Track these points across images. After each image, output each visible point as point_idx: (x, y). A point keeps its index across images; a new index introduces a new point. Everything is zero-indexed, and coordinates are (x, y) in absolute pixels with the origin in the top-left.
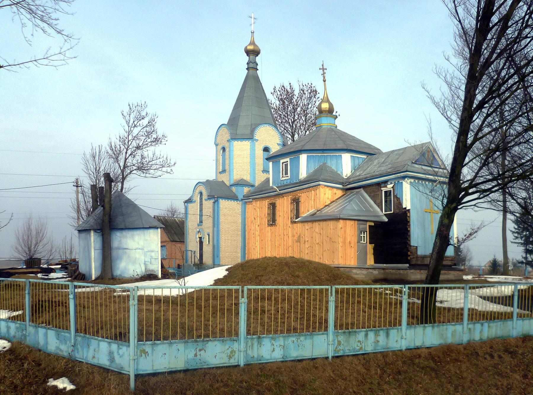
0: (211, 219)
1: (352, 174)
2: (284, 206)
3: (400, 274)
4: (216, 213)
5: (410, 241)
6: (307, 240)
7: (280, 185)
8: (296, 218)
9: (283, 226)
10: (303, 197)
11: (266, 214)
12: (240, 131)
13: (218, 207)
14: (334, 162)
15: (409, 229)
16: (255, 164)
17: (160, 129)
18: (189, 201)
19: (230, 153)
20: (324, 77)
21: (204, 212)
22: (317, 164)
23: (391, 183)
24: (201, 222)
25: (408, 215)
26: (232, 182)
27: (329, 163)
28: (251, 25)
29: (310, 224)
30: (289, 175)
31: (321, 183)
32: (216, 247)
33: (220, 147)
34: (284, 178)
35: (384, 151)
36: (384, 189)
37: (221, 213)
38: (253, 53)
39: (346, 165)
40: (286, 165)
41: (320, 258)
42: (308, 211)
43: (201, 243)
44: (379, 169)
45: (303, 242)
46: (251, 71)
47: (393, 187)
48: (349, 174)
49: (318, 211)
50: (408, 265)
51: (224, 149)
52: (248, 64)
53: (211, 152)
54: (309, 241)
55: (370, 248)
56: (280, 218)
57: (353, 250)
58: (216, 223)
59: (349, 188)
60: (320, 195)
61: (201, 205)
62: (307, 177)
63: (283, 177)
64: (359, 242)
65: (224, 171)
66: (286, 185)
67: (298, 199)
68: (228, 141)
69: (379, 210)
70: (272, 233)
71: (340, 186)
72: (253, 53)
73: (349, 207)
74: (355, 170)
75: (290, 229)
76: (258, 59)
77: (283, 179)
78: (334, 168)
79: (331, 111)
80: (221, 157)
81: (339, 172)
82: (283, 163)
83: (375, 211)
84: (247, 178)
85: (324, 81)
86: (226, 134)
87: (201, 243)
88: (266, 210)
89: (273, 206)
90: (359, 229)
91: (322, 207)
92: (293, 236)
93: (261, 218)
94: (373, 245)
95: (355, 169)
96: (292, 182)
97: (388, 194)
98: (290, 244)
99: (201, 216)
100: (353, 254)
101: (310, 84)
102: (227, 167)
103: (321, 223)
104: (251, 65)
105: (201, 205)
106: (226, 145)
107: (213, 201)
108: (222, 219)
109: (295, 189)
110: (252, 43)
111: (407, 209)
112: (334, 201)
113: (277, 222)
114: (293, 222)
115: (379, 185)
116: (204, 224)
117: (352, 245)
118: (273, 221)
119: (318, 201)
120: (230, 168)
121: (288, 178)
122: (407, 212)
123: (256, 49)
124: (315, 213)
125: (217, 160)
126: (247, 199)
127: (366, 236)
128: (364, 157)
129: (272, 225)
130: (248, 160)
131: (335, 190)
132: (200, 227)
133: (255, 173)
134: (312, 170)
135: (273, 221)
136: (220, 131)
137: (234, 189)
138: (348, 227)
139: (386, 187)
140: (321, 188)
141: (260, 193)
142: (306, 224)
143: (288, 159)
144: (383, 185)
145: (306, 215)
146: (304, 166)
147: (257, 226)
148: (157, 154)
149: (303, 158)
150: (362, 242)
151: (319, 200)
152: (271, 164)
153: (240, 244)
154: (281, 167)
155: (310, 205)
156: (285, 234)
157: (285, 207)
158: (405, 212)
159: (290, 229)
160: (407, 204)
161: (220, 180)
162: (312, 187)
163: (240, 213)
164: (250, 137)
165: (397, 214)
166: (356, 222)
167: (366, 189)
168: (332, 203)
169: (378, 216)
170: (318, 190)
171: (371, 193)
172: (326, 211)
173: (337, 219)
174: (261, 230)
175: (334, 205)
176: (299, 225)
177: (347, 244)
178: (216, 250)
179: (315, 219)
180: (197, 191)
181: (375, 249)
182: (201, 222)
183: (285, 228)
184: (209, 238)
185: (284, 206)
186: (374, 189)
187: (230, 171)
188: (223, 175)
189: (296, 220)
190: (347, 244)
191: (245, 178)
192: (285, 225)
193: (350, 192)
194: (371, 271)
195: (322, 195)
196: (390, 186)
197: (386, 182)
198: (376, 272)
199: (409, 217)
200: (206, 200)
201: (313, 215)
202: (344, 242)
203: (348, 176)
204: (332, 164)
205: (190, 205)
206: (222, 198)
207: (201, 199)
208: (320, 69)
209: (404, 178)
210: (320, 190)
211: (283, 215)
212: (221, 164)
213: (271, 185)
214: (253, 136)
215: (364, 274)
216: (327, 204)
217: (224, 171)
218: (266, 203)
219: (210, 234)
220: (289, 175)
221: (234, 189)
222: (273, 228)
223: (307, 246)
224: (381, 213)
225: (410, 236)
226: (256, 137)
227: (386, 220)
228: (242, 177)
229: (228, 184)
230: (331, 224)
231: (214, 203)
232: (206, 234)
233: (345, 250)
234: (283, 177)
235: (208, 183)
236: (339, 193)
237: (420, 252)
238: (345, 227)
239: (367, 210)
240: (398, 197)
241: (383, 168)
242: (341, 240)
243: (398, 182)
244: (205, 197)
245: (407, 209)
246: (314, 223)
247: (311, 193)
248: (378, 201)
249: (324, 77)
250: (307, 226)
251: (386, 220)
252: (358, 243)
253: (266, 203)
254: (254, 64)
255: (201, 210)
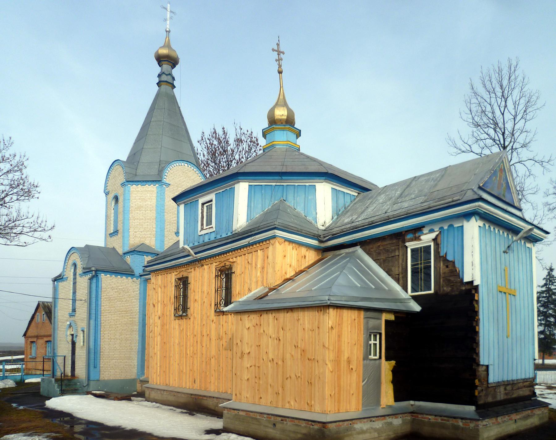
0: (86, 305)
1: (335, 222)
2: (204, 281)
3: (456, 428)
4: (94, 295)
5: (478, 354)
6: (247, 351)
7: (196, 244)
8: (226, 305)
9: (202, 320)
10: (240, 264)
11: (173, 297)
12: (142, 170)
13: (97, 286)
14: (300, 198)
15: (477, 329)
16: (165, 221)
17: (32, 174)
18: (58, 279)
19: (124, 204)
20: (280, 66)
21: (79, 296)
22: (267, 202)
23: (432, 231)
24: (74, 310)
25: (476, 298)
26: (127, 249)
27: (290, 202)
28: (165, 20)
29: (254, 318)
30: (214, 224)
31: (278, 233)
32: (92, 351)
33: (111, 196)
34: (206, 232)
35: (380, 187)
36: (411, 245)
37: (104, 296)
38: (167, 60)
39: (323, 206)
40: (210, 208)
41: (277, 394)
42: (250, 290)
43: (73, 344)
44: (396, 207)
45: (239, 355)
46: (163, 87)
47: (435, 240)
48: (329, 222)
49: (271, 290)
50: (473, 408)
51: (116, 198)
52: (159, 76)
53: (98, 205)
54: (252, 354)
55: (387, 368)
56: (196, 304)
57: (354, 376)
58: (94, 313)
59: (329, 247)
60: (274, 258)
61: (75, 283)
62: (247, 226)
63: (202, 229)
64: (366, 358)
65: (116, 232)
66: (208, 244)
67: (231, 268)
68: (123, 185)
69: (397, 288)
70: (181, 331)
71: (314, 242)
72: (167, 60)
73: (341, 281)
74: (338, 215)
75: (213, 326)
76: (175, 72)
77: (204, 232)
78: (300, 209)
79: (289, 122)
80: (113, 211)
81: (310, 218)
82: (203, 204)
83: (391, 290)
84: (151, 242)
85: (280, 72)
86: (120, 176)
87: (73, 344)
88: (171, 291)
89: (184, 283)
90: (367, 328)
91: (278, 283)
92: (220, 338)
93: (165, 305)
94: (393, 363)
95: (338, 214)
96: (219, 237)
97: (421, 254)
98: (213, 353)
99: (74, 301)
100: (354, 385)
101: (250, 132)
102: (120, 227)
103: (281, 316)
104: (164, 78)
105: (75, 283)
106: (120, 192)
107: (89, 276)
108: (105, 305)
109: (223, 251)
110: (167, 45)
111: (475, 284)
112: (301, 272)
113: (190, 312)
114: (219, 313)
115: (399, 237)
116: (77, 313)
117: (353, 366)
118: (182, 309)
119: (270, 271)
120: (123, 226)
121: (211, 230)
122: (473, 292)
123: (172, 54)
124: (266, 295)
125: (107, 217)
126: (148, 272)
127: (379, 344)
128: (353, 193)
129: (181, 317)
130: (153, 214)
131: (303, 250)
132: (72, 318)
133: (163, 236)
134: (257, 214)
135: (182, 309)
136: (113, 173)
137: (129, 259)
138: (345, 325)
139: (418, 239)
140: (277, 244)
141: (163, 262)
142: (245, 317)
143: (212, 196)
144: (409, 236)
145: (244, 298)
146: (243, 205)
147: (157, 318)
148: (23, 212)
149: (242, 189)
150: (372, 357)
151: (274, 268)
152: (182, 207)
153: (136, 346)
154: (200, 211)
155: (254, 280)
156: (205, 334)
157: (206, 284)
158: (470, 290)
159: (213, 326)
160: (472, 271)
161: (110, 246)
162: (259, 242)
163: (138, 297)
164: (158, 180)
165: (446, 295)
166: (362, 313)
167: (368, 247)
168: (298, 274)
169: (401, 301)
170: (271, 248)
171: (379, 254)
172: (287, 290)
173: (323, 307)
174: (163, 325)
175: (303, 278)
176: (231, 318)
177: (344, 364)
178: (92, 356)
179: (264, 306)
180: (71, 262)
181: (394, 371)
182: (74, 310)
183: (204, 323)
184: (84, 336)
185: (204, 281)
186: (386, 246)
187: (123, 232)
188: (115, 238)
189: (225, 309)
190: (344, 364)
191: (147, 242)
192: (205, 318)
193: (330, 254)
194: (389, 420)
195: (279, 259)
196: (427, 238)
197: (417, 230)
198: (397, 422)
199: (477, 302)
200: (81, 276)
201: (261, 298)
202: (337, 361)
203: (327, 225)
204: (296, 202)
205: (61, 285)
206: (106, 272)
207: (75, 274)
208: (273, 50)
209: (467, 216)
210: (274, 249)
211: (202, 299)
212: (112, 223)
213: (181, 245)
214: (161, 177)
215: (376, 430)
216: (288, 276)
217: (116, 232)
218: (172, 277)
219: (85, 331)
220: (214, 224)
221: (129, 259)
222: (183, 322)
223: (247, 363)
224: (403, 295)
225: (478, 344)
226: (166, 180)
227: (416, 308)
228: (142, 241)
229: (120, 252)
230: (307, 318)
231: (91, 279)
232: (80, 330)
233: (339, 378)
234: (202, 229)
235: (88, 251)
236: (311, 256)
237: (492, 379)
238: (340, 325)
239: (378, 288)
240: (450, 258)
241: (406, 205)
242: (330, 356)
243: (451, 226)
244: (79, 271)
245: (475, 284)
246: (265, 316)
247: (257, 256)
248: (396, 270)
249: (280, 66)
250: (249, 321)
251: (416, 308)
252: (364, 359)
253: (172, 277)
254: (169, 77)
255: (74, 293)
